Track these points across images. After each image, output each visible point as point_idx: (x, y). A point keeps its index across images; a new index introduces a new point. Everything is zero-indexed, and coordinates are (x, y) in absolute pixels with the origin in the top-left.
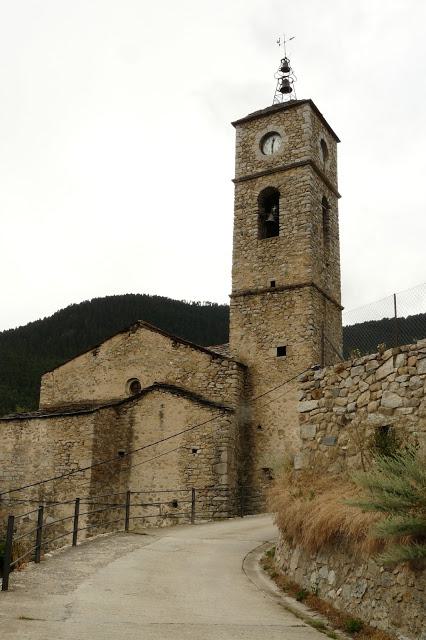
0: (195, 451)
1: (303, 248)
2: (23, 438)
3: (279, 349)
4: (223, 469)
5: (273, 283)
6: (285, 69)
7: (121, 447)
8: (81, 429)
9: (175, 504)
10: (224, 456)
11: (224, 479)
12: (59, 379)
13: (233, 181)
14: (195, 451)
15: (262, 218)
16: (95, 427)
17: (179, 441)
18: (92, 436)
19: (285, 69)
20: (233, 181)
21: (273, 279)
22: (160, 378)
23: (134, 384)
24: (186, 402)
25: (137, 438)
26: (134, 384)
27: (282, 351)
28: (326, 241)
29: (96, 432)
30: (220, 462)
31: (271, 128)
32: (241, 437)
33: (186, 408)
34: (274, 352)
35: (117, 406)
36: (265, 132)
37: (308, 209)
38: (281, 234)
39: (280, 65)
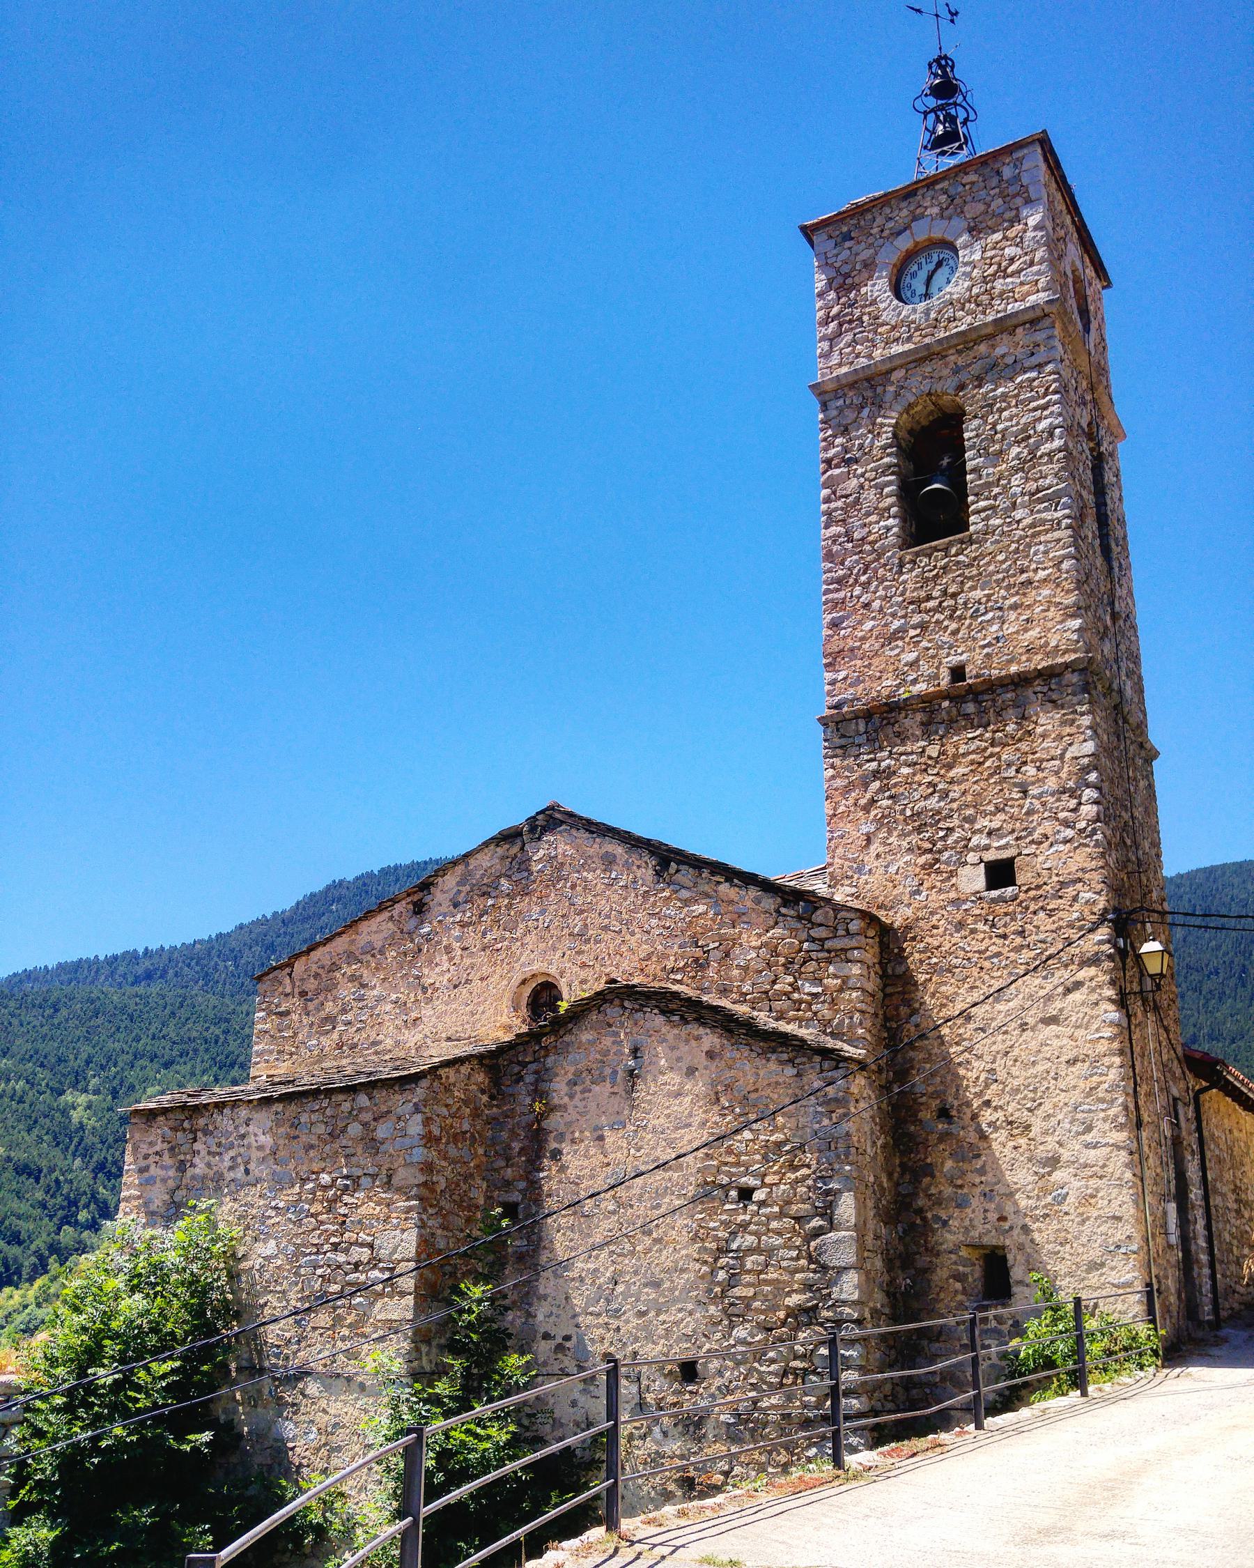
0: (746, 1194)
1: (1053, 552)
2: (200, 1169)
3: (1010, 862)
4: (841, 1246)
5: (958, 673)
6: (946, 89)
7: (507, 1184)
8: (382, 1131)
9: (689, 1372)
10: (847, 1207)
11: (849, 1287)
12: (311, 985)
13: (824, 721)
14: (746, 1194)
15: (908, 493)
16: (427, 1121)
17: (687, 1178)
18: (419, 1154)
19: (946, 89)
20: (824, 721)
21: (954, 660)
22: (627, 970)
23: (542, 996)
24: (710, 1039)
25: (556, 1155)
26: (542, 996)
27: (1000, 874)
28: (1106, 551)
29: (429, 1140)
30: (832, 1227)
31: (921, 232)
32: (884, 1147)
33: (711, 1055)
34: (973, 879)
35: (498, 1064)
36: (904, 243)
37: (1057, 443)
38: (976, 523)
39: (927, 80)
